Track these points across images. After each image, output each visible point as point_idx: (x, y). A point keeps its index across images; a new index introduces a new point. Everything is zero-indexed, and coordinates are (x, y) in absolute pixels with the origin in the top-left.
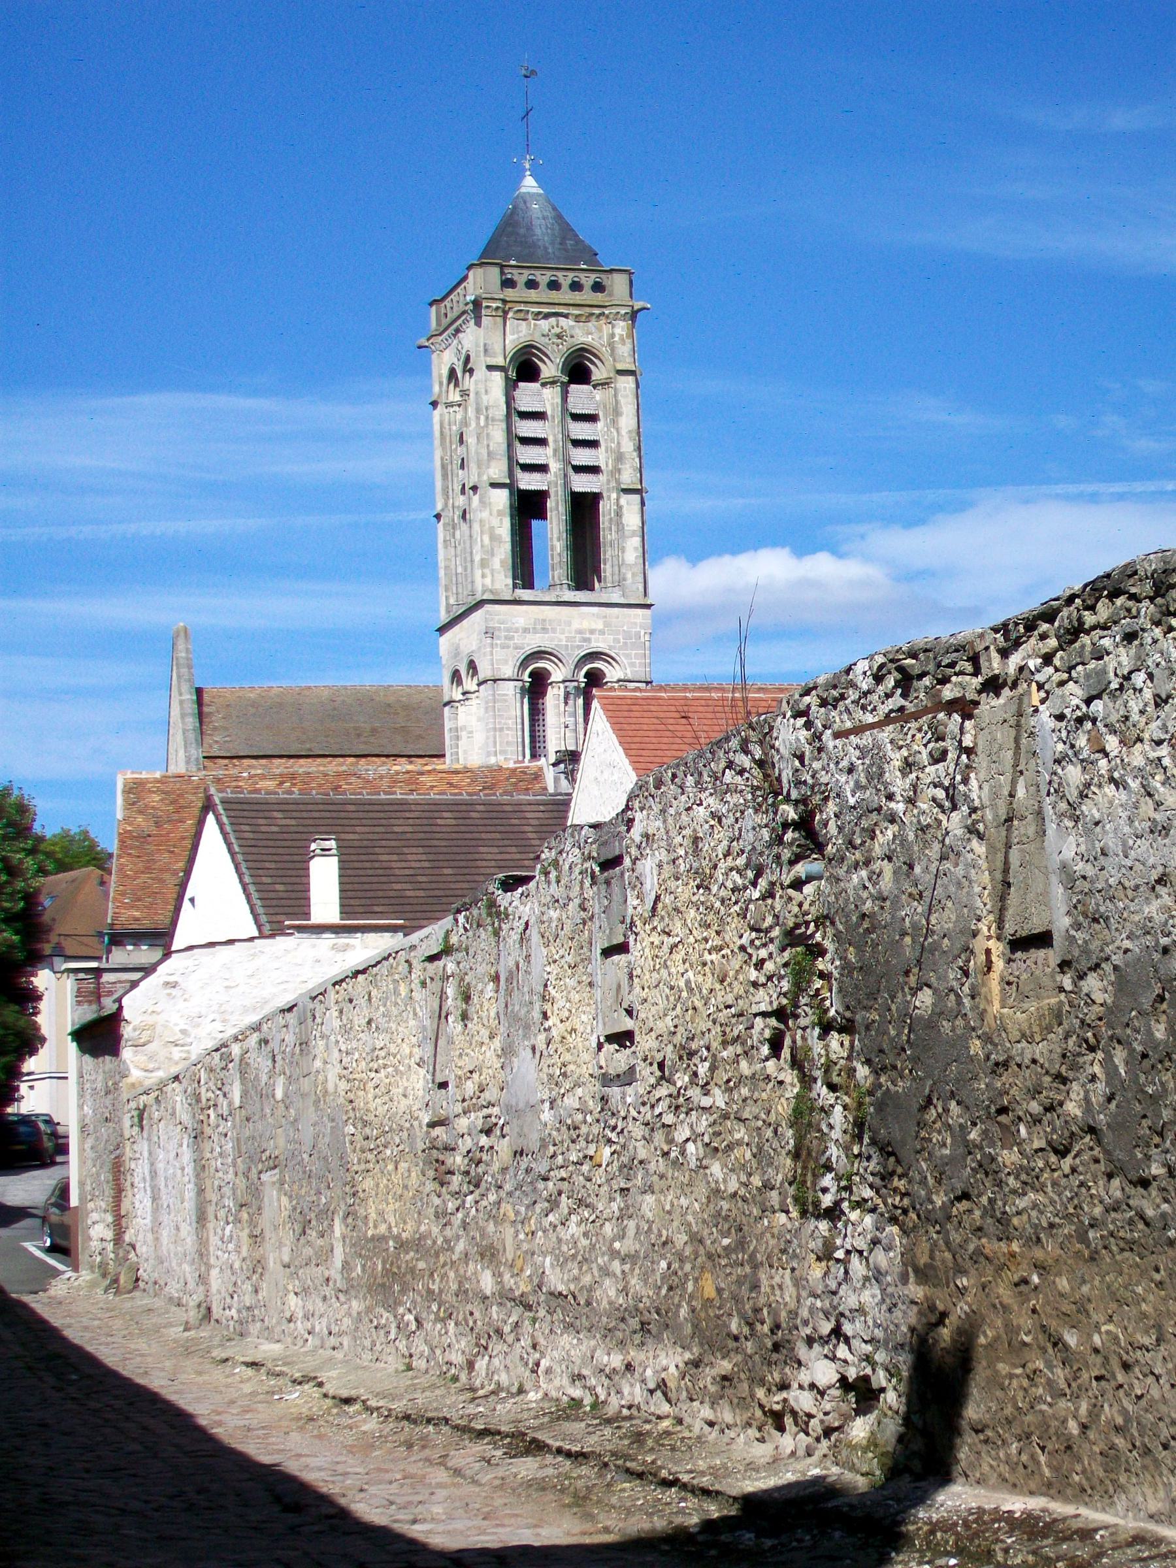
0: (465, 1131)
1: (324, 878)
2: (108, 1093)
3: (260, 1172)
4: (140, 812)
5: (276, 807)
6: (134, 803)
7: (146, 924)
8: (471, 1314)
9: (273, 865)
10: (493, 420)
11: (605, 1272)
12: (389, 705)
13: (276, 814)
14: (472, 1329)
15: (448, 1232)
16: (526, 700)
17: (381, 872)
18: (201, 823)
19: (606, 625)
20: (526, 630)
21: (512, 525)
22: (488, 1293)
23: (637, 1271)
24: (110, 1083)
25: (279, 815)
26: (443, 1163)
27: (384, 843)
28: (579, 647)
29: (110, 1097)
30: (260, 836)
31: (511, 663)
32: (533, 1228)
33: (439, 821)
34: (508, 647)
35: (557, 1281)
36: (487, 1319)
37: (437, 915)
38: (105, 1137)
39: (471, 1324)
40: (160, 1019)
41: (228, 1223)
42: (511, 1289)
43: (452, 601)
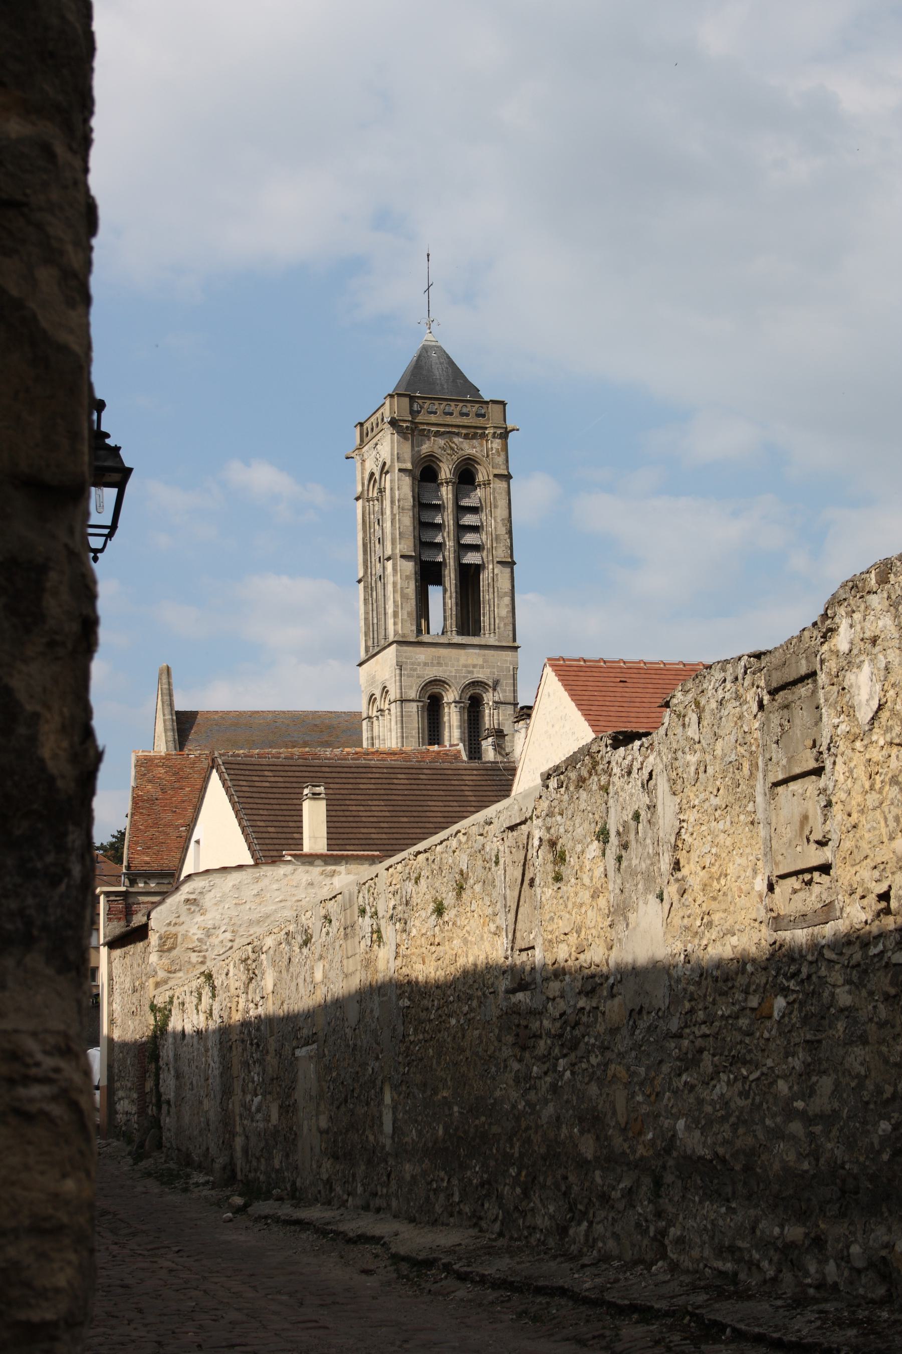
0: (557, 993)
1: (314, 817)
2: (135, 991)
3: (294, 1049)
4: (150, 781)
5: (268, 768)
6: (145, 775)
7: (155, 867)
8: (565, 1178)
9: (265, 812)
10: (403, 509)
11: (777, 1134)
12: (316, 725)
13: (266, 773)
14: (565, 1194)
15: (532, 1096)
16: (426, 714)
17: (351, 819)
18: (206, 780)
19: (485, 661)
20: (426, 664)
21: (416, 586)
22: (590, 1157)
23: (835, 1132)
24: (137, 984)
25: (270, 774)
26: (526, 1027)
27: (352, 797)
28: (465, 677)
29: (137, 994)
30: (255, 789)
31: (415, 688)
32: (658, 1089)
33: (395, 781)
34: (413, 676)
35: (693, 1142)
36: (587, 1184)
37: (487, 804)
38: (132, 1027)
39: (563, 1188)
40: (181, 930)
41: (256, 1096)
42: (624, 1153)
43: (370, 643)
